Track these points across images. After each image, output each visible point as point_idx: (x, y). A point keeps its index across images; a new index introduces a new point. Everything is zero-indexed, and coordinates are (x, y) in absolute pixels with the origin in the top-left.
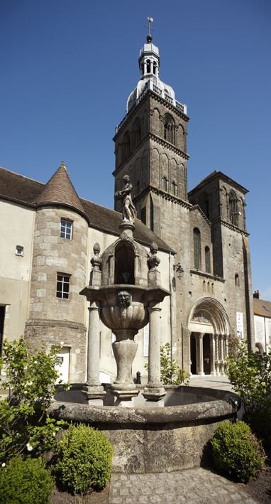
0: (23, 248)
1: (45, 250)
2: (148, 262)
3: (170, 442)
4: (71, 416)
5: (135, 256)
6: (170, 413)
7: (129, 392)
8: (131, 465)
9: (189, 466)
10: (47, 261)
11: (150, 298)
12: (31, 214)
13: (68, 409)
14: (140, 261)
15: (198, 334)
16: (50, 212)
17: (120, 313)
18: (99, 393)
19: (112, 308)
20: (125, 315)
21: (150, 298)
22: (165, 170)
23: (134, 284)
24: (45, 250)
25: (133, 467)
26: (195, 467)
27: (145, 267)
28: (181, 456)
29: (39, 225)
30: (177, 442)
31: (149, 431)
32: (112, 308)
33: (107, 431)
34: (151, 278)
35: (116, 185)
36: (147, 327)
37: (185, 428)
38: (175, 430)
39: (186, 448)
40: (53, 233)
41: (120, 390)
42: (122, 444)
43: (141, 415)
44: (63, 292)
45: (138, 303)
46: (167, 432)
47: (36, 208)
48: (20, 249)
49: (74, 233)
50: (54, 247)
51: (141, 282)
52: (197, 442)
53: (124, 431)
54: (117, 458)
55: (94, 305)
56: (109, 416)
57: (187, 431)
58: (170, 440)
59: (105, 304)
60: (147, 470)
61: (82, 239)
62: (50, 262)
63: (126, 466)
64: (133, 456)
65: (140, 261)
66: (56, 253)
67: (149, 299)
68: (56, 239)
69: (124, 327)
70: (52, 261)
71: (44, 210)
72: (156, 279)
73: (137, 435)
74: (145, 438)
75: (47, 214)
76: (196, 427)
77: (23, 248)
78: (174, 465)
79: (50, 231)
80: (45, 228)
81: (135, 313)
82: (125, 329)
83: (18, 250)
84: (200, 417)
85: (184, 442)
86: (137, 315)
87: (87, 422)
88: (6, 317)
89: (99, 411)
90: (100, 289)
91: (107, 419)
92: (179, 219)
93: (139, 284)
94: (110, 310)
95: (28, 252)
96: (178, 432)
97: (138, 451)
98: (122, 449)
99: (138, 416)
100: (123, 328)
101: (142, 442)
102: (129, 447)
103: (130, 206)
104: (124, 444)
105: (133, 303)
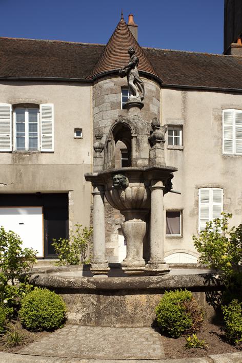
0: (81, 129)
1: (105, 127)
3: (121, 306)
4: (42, 283)
5: (132, 137)
6: (118, 282)
7: (135, 268)
8: (84, 320)
9: (138, 325)
11: (150, 178)
12: (87, 91)
13: (41, 278)
14: (138, 141)
15: (29, 133)
16: (108, 84)
17: (119, 195)
18: (102, 269)
19: (111, 191)
20: (124, 197)
21: (150, 178)
23: (130, 165)
24: (105, 127)
25: (86, 321)
26: (145, 326)
27: (145, 145)
28: (131, 317)
29: (97, 100)
30: (128, 306)
31: (101, 296)
32: (111, 191)
33: (69, 295)
34: (152, 156)
35: (226, 10)
37: (138, 296)
38: (127, 296)
39: (137, 311)
40: (114, 106)
41: (126, 267)
42: (79, 304)
43: (91, 282)
45: (138, 184)
46: (119, 297)
47: (92, 83)
48: (78, 131)
51: (140, 162)
52: (152, 308)
53: (81, 295)
54: (75, 314)
55: (97, 190)
56: (67, 283)
57: (142, 298)
58: (122, 304)
59: (106, 188)
60: (98, 324)
61: (151, 105)
63: (80, 320)
64: (87, 314)
65: (138, 141)
67: (150, 179)
69: (127, 207)
71: (101, 83)
73: (92, 298)
74: (98, 301)
75: (105, 86)
76: (152, 295)
77: (81, 129)
78: (122, 323)
81: (134, 194)
82: (129, 209)
83: (77, 133)
84: (151, 286)
85: (136, 307)
86: (137, 195)
87: (51, 288)
88: (70, 204)
89: (60, 279)
90: (99, 176)
91: (66, 285)
93: (136, 165)
94: (110, 193)
95: (88, 134)
96: (130, 298)
97: (91, 310)
98: (79, 308)
99: (89, 283)
100: (126, 209)
102: (85, 306)
104: (80, 305)
105: (131, 184)
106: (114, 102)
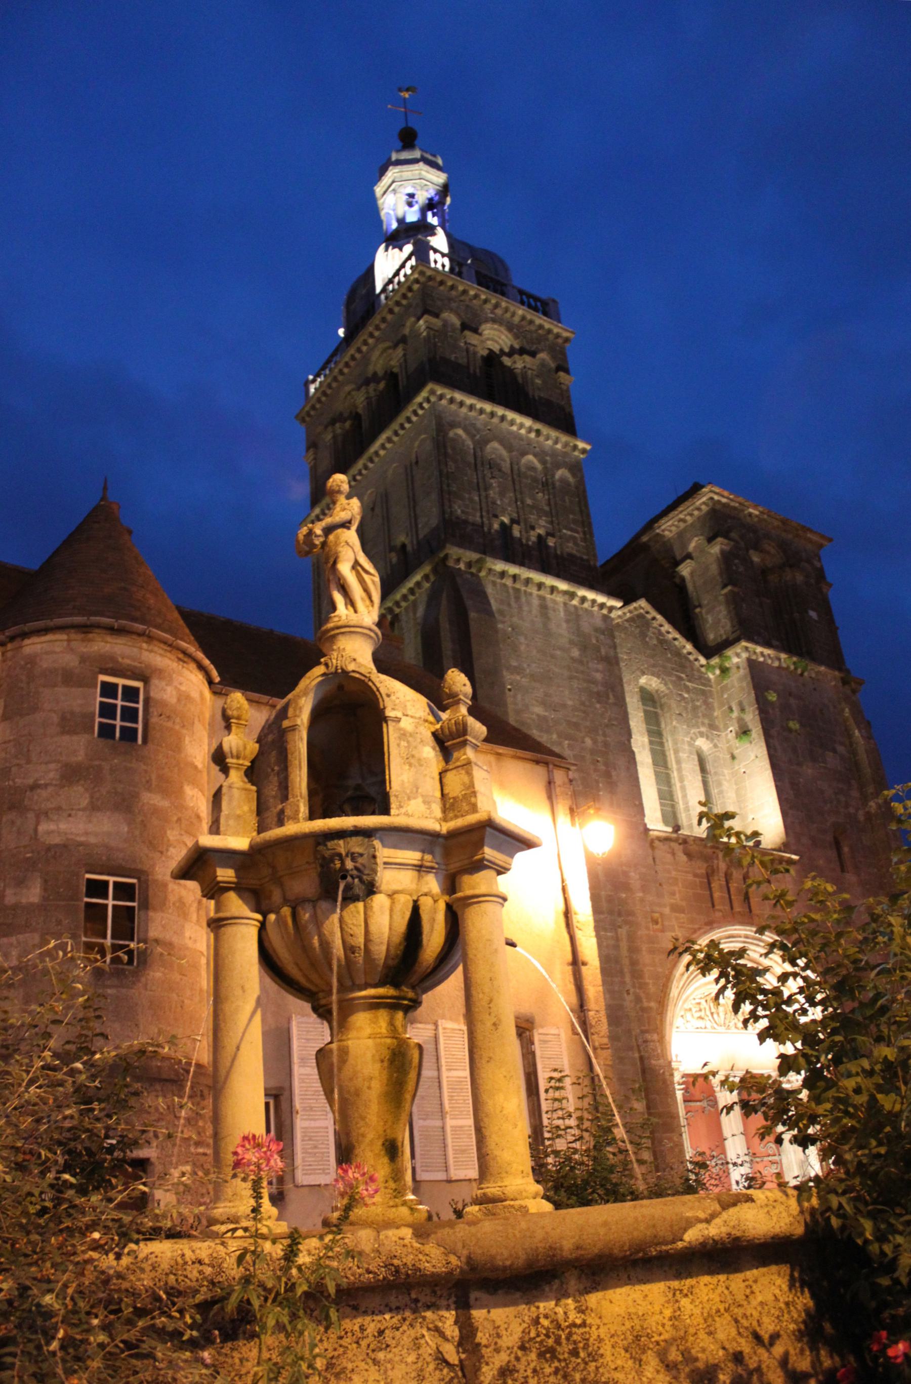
0: (296, 417)
1: (34, 787)
2: (434, 734)
3: (575, 1353)
10: (43, 827)
22: (502, 494)
24: (34, 787)
27: (429, 752)
36: (455, 980)
44: (110, 902)
49: (154, 720)
50: (71, 774)
62: (55, 830)
66: (79, 795)
68: (80, 747)
70: (63, 826)
72: (474, 794)
79: (55, 719)
80: (35, 709)
92: (576, 653)
101: (453, 1359)
103: (356, 565)
106: (72, 713)
